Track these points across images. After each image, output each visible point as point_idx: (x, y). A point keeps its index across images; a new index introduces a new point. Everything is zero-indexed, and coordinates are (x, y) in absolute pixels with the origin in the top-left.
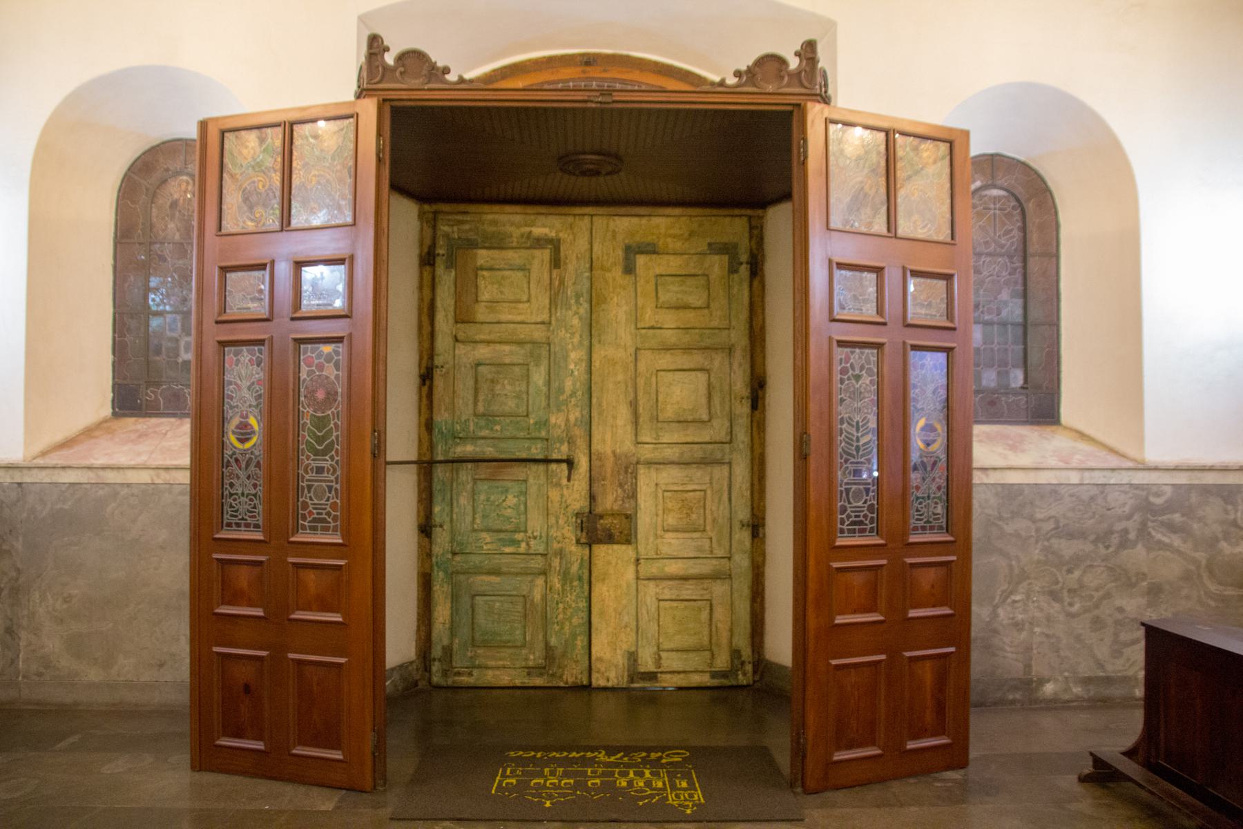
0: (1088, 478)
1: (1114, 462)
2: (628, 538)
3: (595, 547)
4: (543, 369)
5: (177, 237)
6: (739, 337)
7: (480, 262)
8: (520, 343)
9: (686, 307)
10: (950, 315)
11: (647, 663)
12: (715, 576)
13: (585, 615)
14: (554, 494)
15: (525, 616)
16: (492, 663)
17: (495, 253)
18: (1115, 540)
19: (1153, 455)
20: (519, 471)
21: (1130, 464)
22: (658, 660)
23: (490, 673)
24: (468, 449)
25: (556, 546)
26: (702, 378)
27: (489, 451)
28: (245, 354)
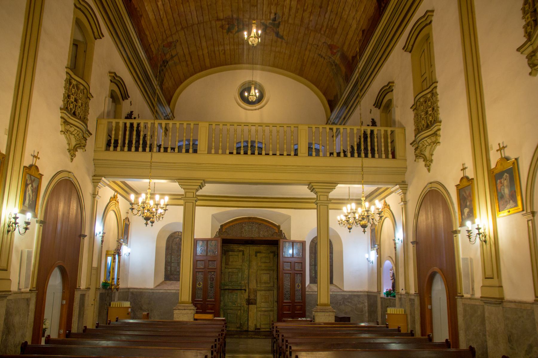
0: (334, 293)
1: (339, 290)
2: (255, 304)
3: (249, 305)
4: (241, 273)
5: (177, 249)
6: (275, 268)
7: (230, 254)
8: (237, 269)
9: (266, 263)
10: (302, 268)
11: (258, 327)
12: (271, 311)
13: (247, 317)
14: (242, 296)
15: (237, 317)
16: (230, 326)
17: (233, 253)
18: (339, 304)
19: (346, 289)
20: (236, 291)
21: (341, 291)
22: (260, 326)
23: (230, 328)
24: (227, 287)
25: (242, 305)
26: (269, 275)
27: (231, 288)
28: (200, 273)
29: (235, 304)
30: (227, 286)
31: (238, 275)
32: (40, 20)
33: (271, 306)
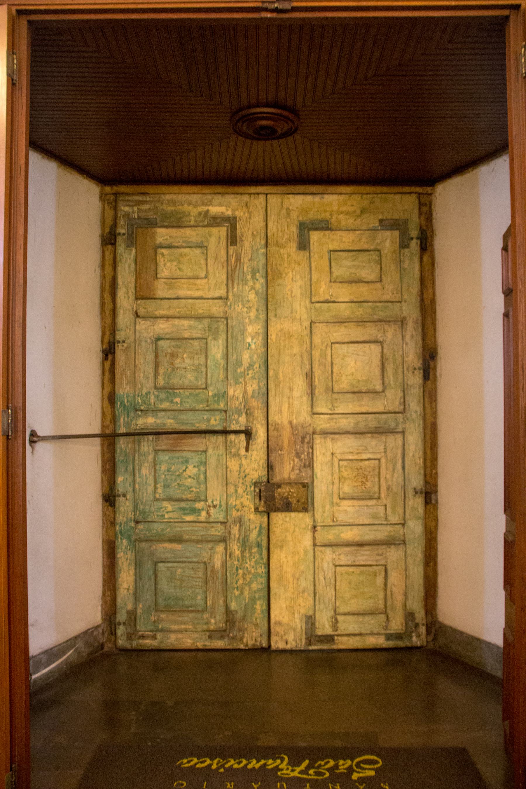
3: (273, 515)
4: (221, 342)
7: (159, 240)
8: (199, 318)
9: (359, 281)
13: (264, 580)
14: (233, 464)
20: (199, 442)
22: (335, 624)
23: (173, 636)
25: (235, 514)
26: (375, 349)
27: (170, 423)
29: (197, 511)
30: (145, 412)
31: (206, 351)
32: (10, 222)
33: (394, 519)
